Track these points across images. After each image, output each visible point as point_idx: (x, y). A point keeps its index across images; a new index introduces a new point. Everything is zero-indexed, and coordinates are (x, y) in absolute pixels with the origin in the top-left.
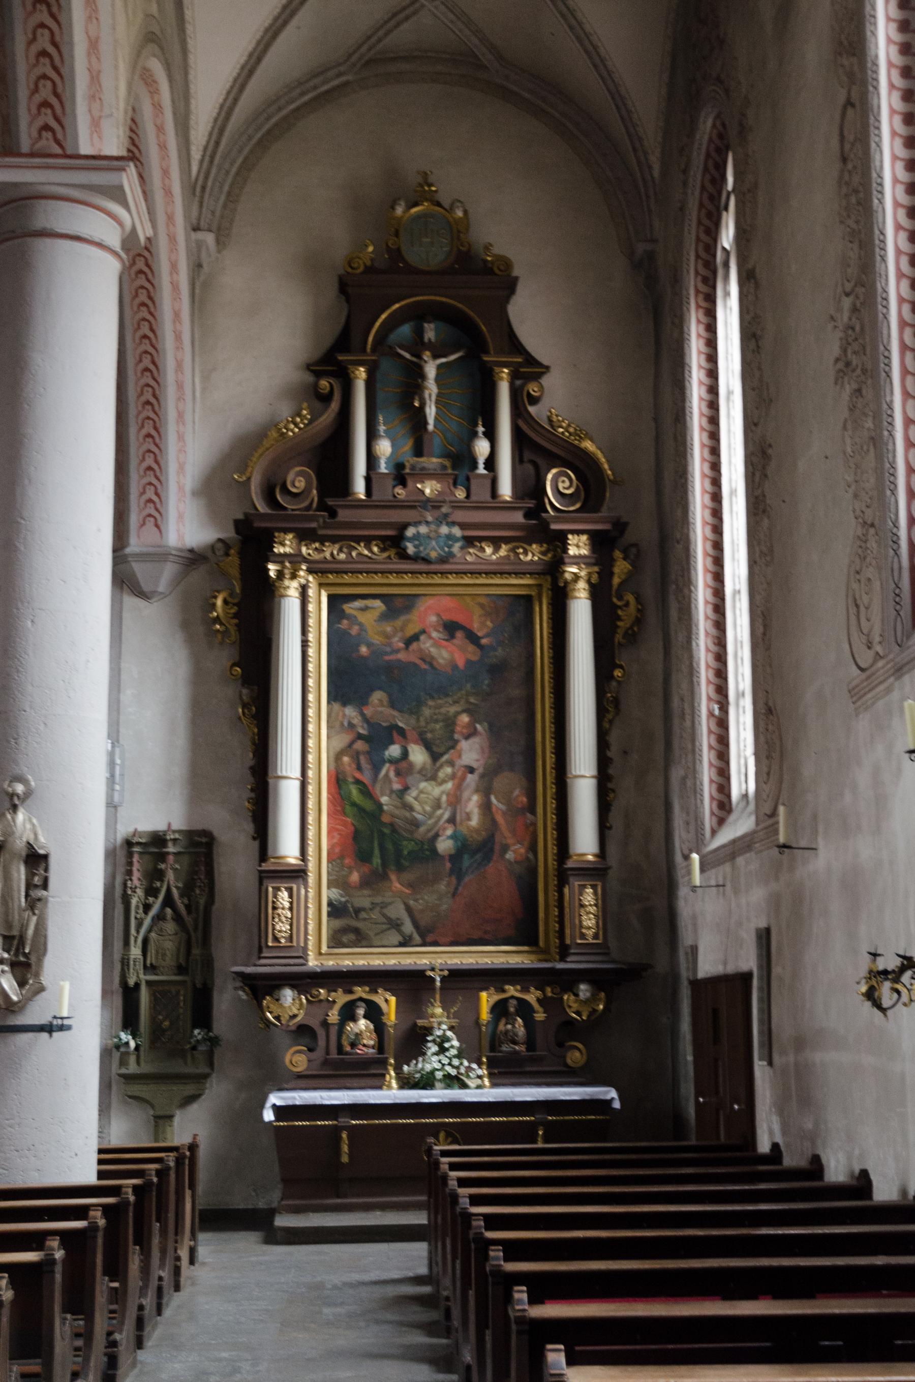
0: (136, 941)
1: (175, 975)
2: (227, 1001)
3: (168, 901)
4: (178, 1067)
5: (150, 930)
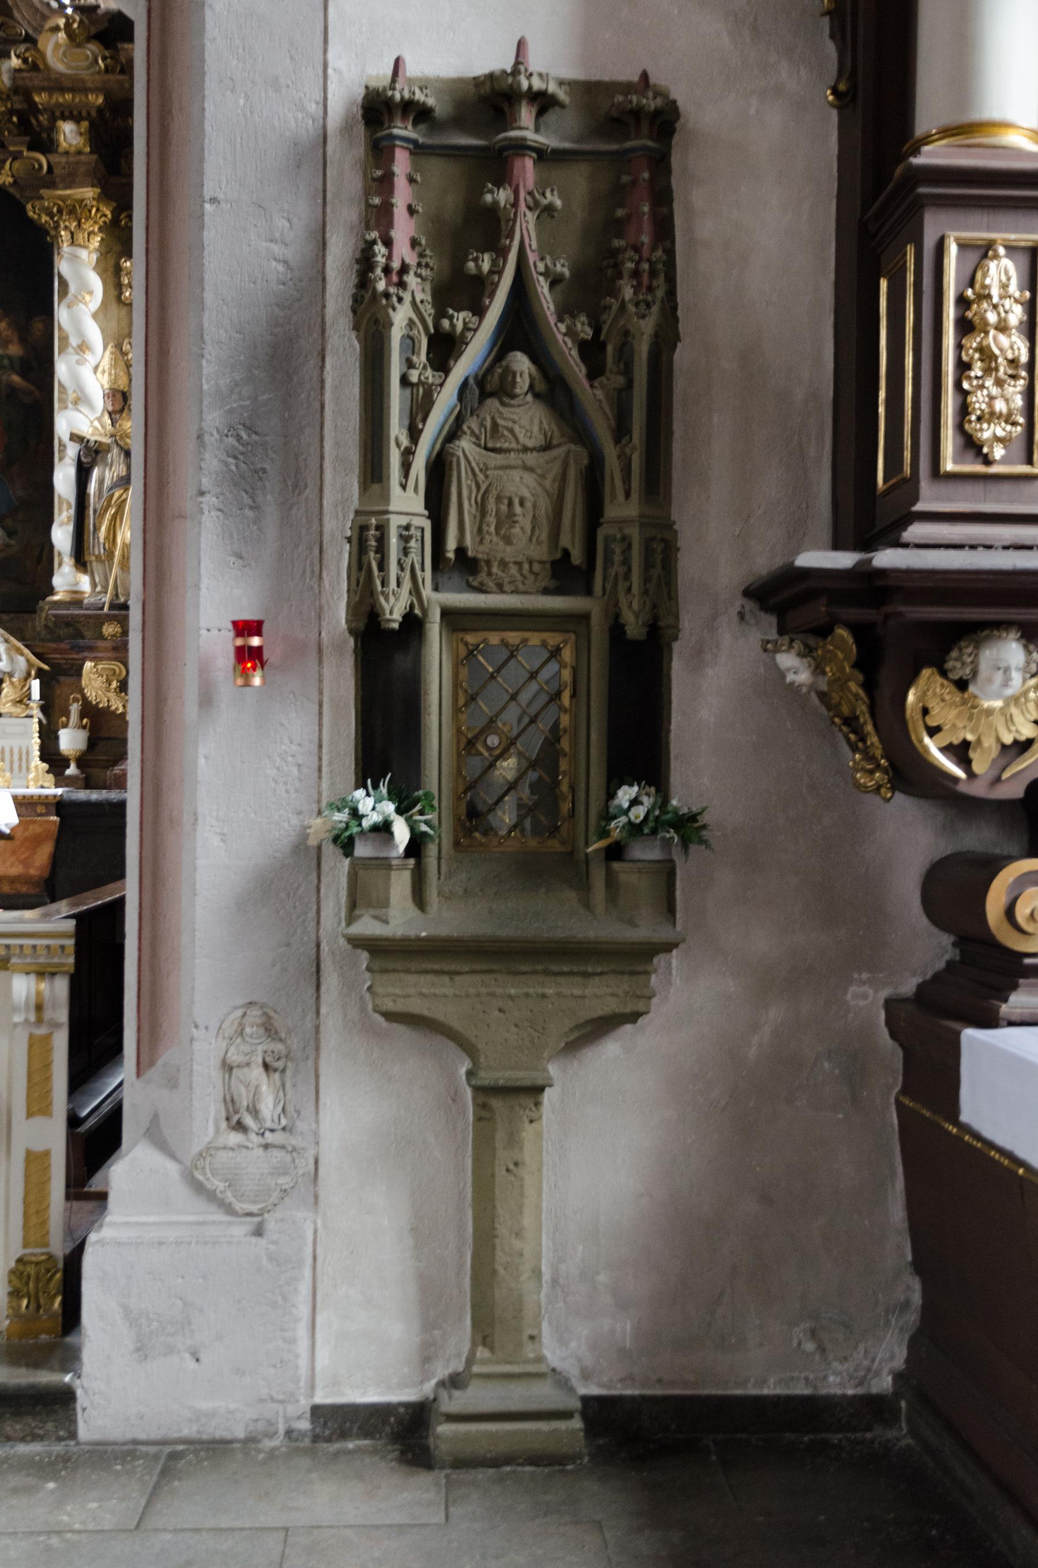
0: (406, 467)
1: (546, 591)
2: (725, 688)
3: (519, 329)
4: (559, 915)
5: (453, 434)
